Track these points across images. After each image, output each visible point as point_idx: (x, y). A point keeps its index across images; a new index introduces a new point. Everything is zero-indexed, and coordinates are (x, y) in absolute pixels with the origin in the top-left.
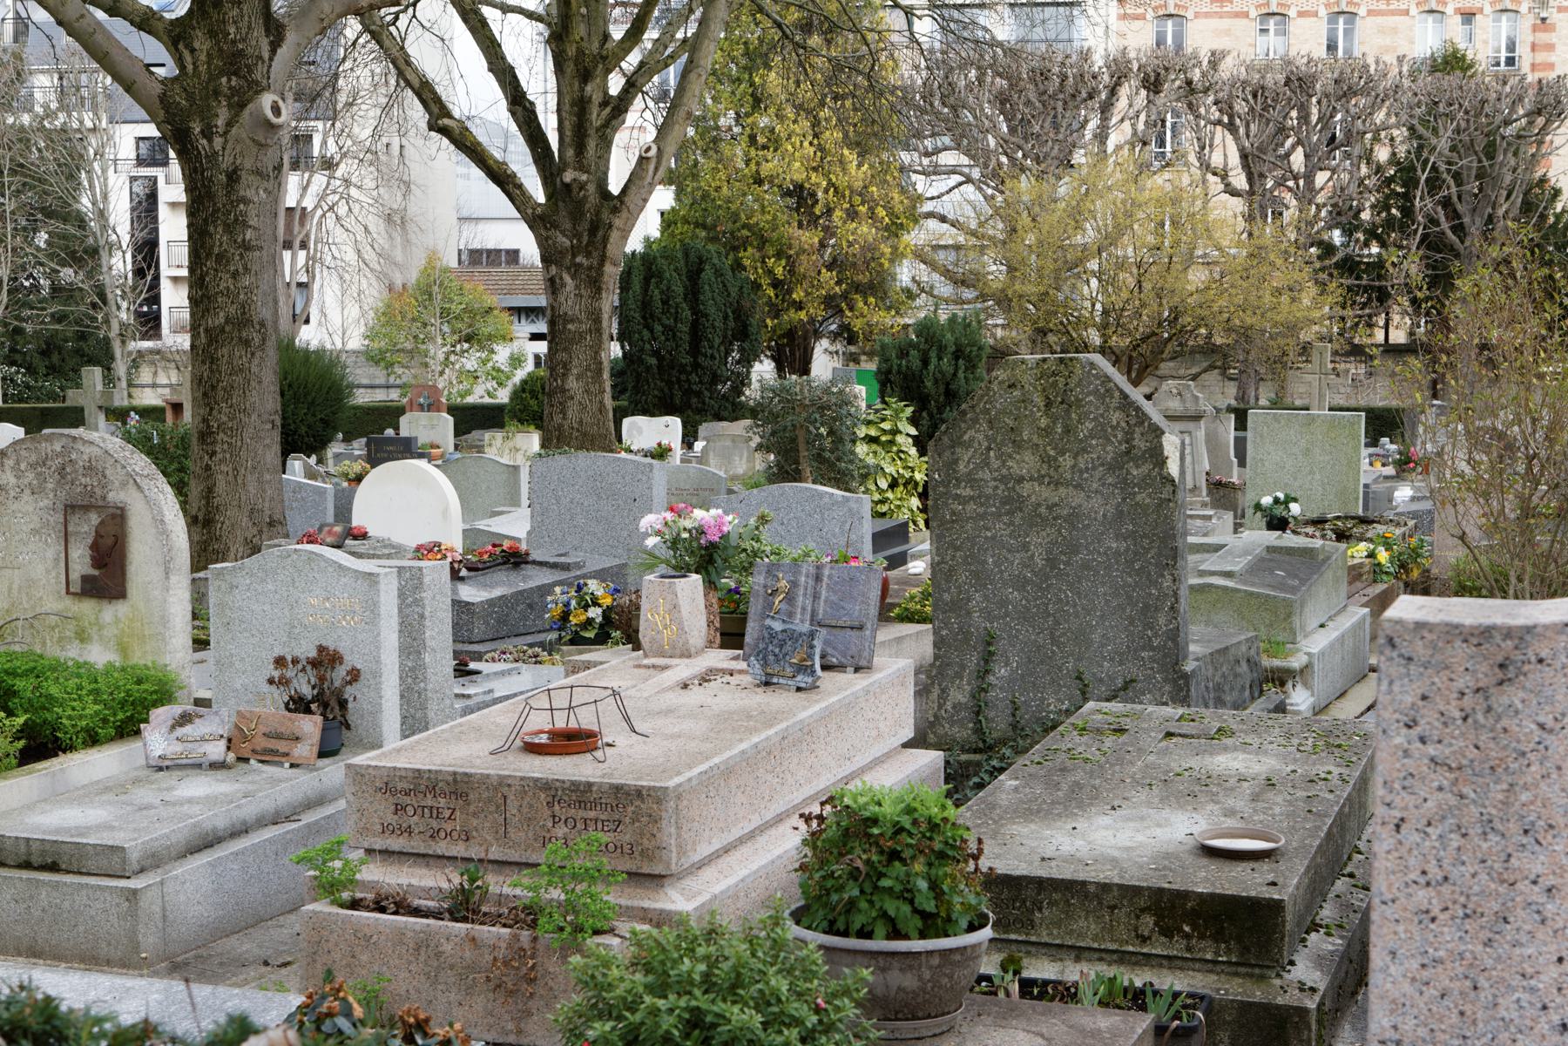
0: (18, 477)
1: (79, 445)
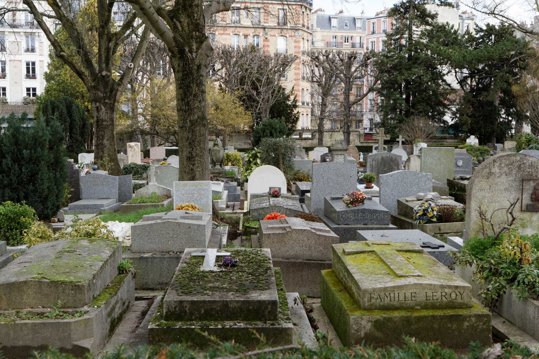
0: (500, 170)
1: (528, 158)
